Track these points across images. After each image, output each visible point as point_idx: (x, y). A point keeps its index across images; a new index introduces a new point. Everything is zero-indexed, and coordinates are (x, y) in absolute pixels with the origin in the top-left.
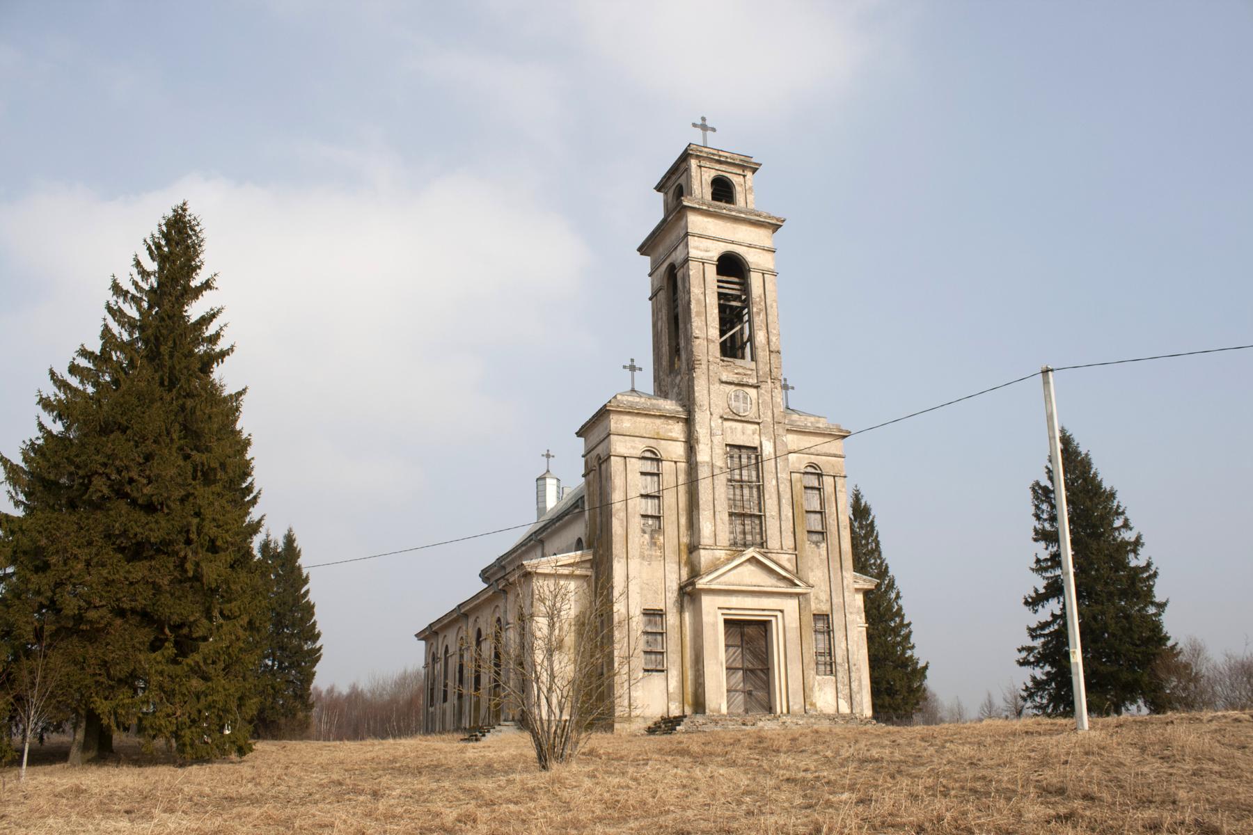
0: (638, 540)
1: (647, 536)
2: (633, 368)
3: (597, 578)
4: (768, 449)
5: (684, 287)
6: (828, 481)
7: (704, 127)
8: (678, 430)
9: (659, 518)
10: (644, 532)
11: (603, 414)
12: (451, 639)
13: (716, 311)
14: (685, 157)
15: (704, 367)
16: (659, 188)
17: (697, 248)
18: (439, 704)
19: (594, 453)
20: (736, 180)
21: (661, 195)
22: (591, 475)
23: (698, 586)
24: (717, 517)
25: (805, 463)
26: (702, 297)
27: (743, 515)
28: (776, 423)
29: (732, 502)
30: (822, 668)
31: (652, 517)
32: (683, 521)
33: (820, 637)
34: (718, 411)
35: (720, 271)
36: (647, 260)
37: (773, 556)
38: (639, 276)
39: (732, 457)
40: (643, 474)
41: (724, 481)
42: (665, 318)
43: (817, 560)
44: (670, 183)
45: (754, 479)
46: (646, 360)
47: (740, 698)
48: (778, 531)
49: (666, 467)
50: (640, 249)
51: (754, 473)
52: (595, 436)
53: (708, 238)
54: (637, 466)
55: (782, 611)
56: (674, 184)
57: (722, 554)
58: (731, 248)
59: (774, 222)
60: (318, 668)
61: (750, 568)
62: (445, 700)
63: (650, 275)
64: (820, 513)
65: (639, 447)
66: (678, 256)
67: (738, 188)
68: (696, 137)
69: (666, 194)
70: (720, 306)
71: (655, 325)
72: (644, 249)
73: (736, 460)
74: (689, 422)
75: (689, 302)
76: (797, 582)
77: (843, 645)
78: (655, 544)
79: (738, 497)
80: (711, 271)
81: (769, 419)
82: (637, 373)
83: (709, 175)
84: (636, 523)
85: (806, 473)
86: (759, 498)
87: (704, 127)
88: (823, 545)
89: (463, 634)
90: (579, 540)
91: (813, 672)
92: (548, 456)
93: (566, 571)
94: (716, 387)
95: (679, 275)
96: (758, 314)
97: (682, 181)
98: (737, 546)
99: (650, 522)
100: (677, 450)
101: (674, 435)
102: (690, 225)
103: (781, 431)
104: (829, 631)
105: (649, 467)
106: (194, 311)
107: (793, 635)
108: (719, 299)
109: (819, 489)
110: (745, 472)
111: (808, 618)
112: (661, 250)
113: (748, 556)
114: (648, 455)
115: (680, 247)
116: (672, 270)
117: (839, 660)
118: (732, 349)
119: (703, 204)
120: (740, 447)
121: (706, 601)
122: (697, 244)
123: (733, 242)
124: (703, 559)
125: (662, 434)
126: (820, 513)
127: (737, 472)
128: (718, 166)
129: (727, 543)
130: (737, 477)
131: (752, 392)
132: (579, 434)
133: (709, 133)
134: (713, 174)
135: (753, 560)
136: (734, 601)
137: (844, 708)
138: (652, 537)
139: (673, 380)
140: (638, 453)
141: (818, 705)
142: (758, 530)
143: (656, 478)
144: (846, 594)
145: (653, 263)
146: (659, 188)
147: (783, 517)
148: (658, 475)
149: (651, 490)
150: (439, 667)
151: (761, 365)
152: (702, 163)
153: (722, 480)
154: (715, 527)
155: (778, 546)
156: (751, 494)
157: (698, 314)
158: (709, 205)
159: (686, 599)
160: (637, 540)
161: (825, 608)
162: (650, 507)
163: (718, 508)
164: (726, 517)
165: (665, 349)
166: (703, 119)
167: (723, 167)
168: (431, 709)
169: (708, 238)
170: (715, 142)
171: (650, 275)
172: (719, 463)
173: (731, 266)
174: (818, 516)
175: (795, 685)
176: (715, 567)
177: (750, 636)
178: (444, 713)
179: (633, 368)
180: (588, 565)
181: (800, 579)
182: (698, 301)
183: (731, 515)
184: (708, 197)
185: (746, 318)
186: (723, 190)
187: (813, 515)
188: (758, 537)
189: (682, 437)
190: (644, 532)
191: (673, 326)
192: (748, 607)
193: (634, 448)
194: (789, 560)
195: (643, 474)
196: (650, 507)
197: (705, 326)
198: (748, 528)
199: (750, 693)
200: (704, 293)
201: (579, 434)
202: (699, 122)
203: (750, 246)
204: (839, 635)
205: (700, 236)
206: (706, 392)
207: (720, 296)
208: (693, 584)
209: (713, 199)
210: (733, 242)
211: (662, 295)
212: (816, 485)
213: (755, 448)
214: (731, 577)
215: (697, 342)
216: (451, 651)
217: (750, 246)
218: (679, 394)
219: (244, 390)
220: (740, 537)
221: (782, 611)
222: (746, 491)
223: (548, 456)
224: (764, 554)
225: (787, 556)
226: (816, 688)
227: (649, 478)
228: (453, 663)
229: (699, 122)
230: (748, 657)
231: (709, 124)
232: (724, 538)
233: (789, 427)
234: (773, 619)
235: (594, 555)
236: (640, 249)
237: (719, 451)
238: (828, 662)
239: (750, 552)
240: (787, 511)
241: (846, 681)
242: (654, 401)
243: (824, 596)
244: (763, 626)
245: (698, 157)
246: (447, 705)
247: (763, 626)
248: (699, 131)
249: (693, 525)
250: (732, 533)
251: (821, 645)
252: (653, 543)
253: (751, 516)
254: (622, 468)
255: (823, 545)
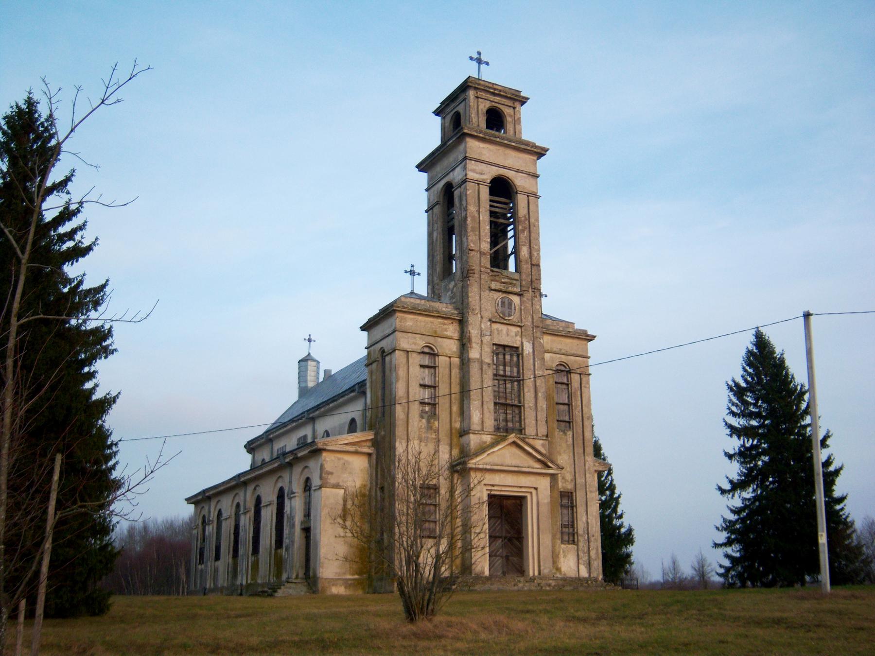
0: (417, 423)
1: (424, 421)
2: (412, 273)
3: (378, 454)
4: (528, 348)
5: (461, 204)
6: (575, 378)
7: (479, 61)
8: (452, 330)
9: (434, 405)
10: (422, 417)
11: (387, 312)
12: (226, 505)
13: (488, 227)
14: (464, 87)
15: (476, 276)
16: (437, 113)
17: (474, 171)
18: (210, 564)
19: (379, 346)
20: (507, 111)
21: (439, 119)
22: (374, 365)
23: (470, 466)
24: (485, 407)
25: (423, 344)
26: (477, 215)
27: (506, 405)
28: (535, 326)
29: (497, 394)
30: (566, 538)
31: (428, 404)
32: (455, 408)
33: (565, 511)
34: (487, 315)
35: (492, 192)
36: (424, 176)
37: (531, 441)
38: (416, 192)
39: (497, 354)
40: (422, 366)
41: (491, 376)
42: (440, 230)
43: (564, 445)
44: (448, 110)
45: (515, 374)
46: (422, 267)
47: (499, 562)
48: (535, 419)
49: (442, 361)
50: (418, 166)
51: (515, 370)
52: (380, 331)
53: (483, 162)
54: (416, 360)
55: (536, 489)
56: (452, 111)
57: (488, 439)
58: (502, 172)
59: (538, 151)
60: (834, 487)
61: (514, 450)
62: (217, 558)
63: (427, 190)
64: (568, 405)
65: (420, 343)
66: (456, 176)
67: (509, 119)
68: (471, 70)
69: (443, 118)
70: (491, 222)
71: (430, 235)
72: (423, 167)
73: (501, 356)
74: (462, 323)
75: (466, 218)
76: (550, 464)
77: (584, 519)
78: (431, 428)
79: (502, 390)
80: (485, 192)
81: (529, 324)
82: (416, 277)
83: (484, 106)
84: (415, 409)
85: (423, 353)
86: (519, 391)
87: (479, 61)
88: (570, 433)
89: (240, 499)
90: (353, 421)
91: (559, 542)
92: (310, 340)
93: (352, 449)
94: (486, 294)
95: (456, 193)
96: (523, 231)
97: (460, 109)
98: (502, 432)
99: (427, 409)
100: (450, 346)
101: (449, 333)
102: (468, 150)
103: (539, 334)
104: (572, 507)
105: (426, 361)
106: (51, 207)
107: (545, 510)
108: (491, 216)
109: (567, 385)
110: (508, 369)
111: (557, 495)
112: (439, 169)
113: (511, 441)
114: (427, 350)
115: (458, 169)
116: (449, 189)
117: (581, 531)
118: (498, 260)
119: (481, 132)
120: (504, 346)
121: (475, 477)
122: (473, 167)
123: (504, 167)
124: (472, 442)
125: (439, 332)
126: (568, 405)
127: (501, 368)
128: (492, 98)
129: (492, 429)
130: (501, 373)
131: (516, 299)
132: (364, 328)
133: (483, 66)
134: (488, 105)
135: (514, 443)
136: (497, 479)
137: (584, 573)
138: (428, 422)
139: (446, 287)
140: (418, 348)
141: (563, 569)
142: (517, 419)
143: (432, 370)
144: (588, 475)
145: (430, 179)
146: (437, 113)
147: (539, 409)
148: (434, 368)
149: (427, 382)
150: (210, 529)
151: (524, 277)
152: (480, 94)
153: (489, 373)
154: (482, 414)
155: (534, 433)
156: (512, 386)
157: (473, 230)
158: (486, 134)
159: (456, 476)
160: (416, 424)
161: (570, 487)
162: (426, 394)
163: (486, 399)
164: (492, 406)
165: (439, 257)
166: (479, 53)
167: (497, 99)
168: (199, 567)
169: (483, 162)
170: (489, 75)
171: (427, 190)
172: (488, 360)
173: (501, 188)
174: (566, 407)
175: (546, 552)
176: (483, 449)
177: (508, 512)
178: (216, 570)
179: (412, 273)
180: (369, 444)
181: (552, 462)
182: (473, 218)
183: (495, 404)
184: (483, 125)
185: (511, 234)
186: (495, 120)
187: (561, 407)
188: (518, 424)
189: (456, 335)
190: (422, 417)
191: (447, 237)
192: (507, 484)
193: (415, 344)
194: (543, 445)
195: (422, 366)
196: (426, 394)
197: (479, 240)
198: (509, 416)
199: (507, 558)
200: (477, 209)
201: (364, 328)
202: (475, 56)
203: (518, 171)
204: (581, 510)
205: (477, 160)
206: (477, 298)
207: (492, 214)
208: (464, 463)
209: (488, 127)
210: (504, 167)
211: (437, 209)
212: (565, 381)
213: (517, 348)
214: (489, 459)
215: (472, 253)
216: (225, 515)
217: (518, 171)
218: (452, 298)
219: (107, 280)
220: (502, 424)
221: (536, 489)
222: (509, 385)
223: (310, 340)
224: (523, 440)
225: (541, 442)
226: (561, 555)
227: (427, 370)
228: (228, 527)
229: (475, 56)
230: (507, 527)
231: (484, 58)
232: (490, 423)
233: (544, 330)
234: (528, 495)
235: (376, 435)
236: (418, 166)
237: (487, 349)
238: (569, 533)
239: (512, 437)
240: (543, 404)
241: (586, 550)
242: (432, 304)
243: (569, 477)
244: (519, 502)
245: (476, 88)
246: (219, 563)
247: (519, 502)
248: (475, 64)
249: (463, 412)
250: (496, 420)
251: (566, 519)
252: (429, 428)
253: (512, 405)
254: (404, 360)
255: (570, 433)
